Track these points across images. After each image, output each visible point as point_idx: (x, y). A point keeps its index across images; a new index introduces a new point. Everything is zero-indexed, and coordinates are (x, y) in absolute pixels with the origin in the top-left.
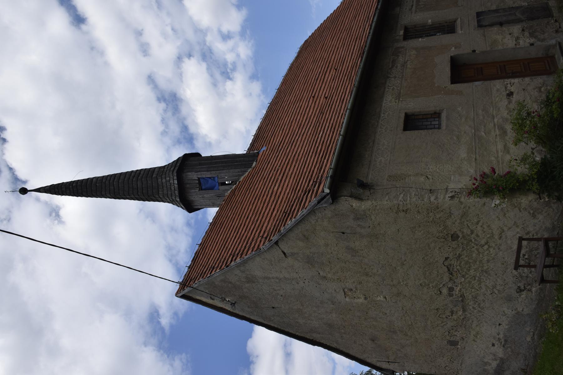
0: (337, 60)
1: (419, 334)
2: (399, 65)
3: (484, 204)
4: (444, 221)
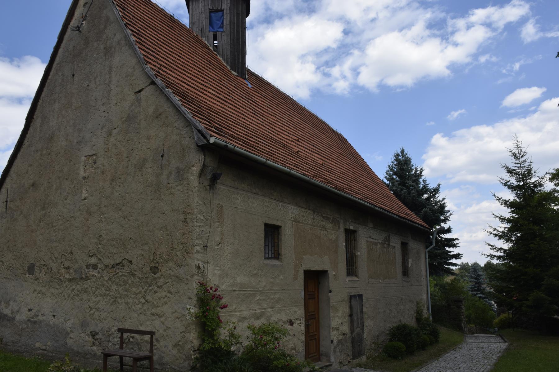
0: (331, 167)
1: (41, 234)
2: (324, 223)
3: (190, 298)
4: (173, 260)
